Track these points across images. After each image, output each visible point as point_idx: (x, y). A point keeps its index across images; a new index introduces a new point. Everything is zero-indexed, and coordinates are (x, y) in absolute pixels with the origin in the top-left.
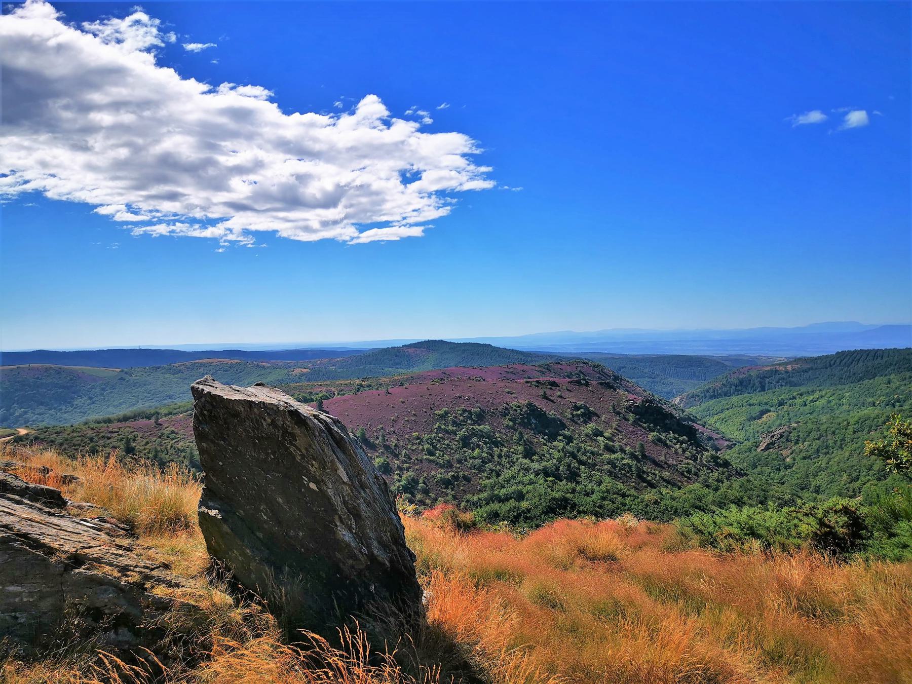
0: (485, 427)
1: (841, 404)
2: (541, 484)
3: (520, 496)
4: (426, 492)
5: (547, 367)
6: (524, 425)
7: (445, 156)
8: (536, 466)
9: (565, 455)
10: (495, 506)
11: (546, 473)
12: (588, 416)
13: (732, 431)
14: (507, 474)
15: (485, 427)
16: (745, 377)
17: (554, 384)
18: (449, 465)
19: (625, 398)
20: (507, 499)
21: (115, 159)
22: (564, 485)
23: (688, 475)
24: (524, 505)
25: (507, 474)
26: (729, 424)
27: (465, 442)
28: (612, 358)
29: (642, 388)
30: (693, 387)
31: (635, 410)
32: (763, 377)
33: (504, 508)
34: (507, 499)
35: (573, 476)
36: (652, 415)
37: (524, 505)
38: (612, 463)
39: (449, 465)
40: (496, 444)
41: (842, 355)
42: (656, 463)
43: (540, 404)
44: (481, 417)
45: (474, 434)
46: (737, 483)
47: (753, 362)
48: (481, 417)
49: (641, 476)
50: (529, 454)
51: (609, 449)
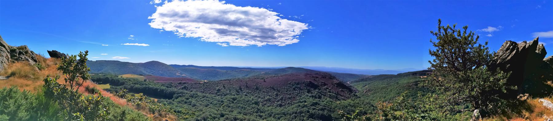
0: (299, 86)
1: (380, 84)
2: (311, 99)
3: (305, 102)
4: (285, 100)
5: (317, 74)
6: (308, 86)
7: (300, 27)
8: (310, 95)
9: (74, 73)
10: (300, 104)
11: (313, 97)
12: (325, 84)
13: (360, 89)
14: (303, 96)
15: (299, 86)
16: (363, 79)
17: (317, 77)
18: (290, 94)
19: (335, 81)
20: (302, 102)
21: (173, 10)
22: (317, 100)
23: (348, 98)
24: (306, 104)
25: (303, 96)
26: (359, 87)
27: (294, 89)
28: (334, 73)
29: (341, 79)
30: (353, 80)
31: (337, 84)
32: (366, 79)
33: (301, 104)
34: (302, 102)
35: (320, 97)
36: (341, 85)
37: (306, 104)
38: (330, 95)
39: (290, 94)
40: (301, 90)
41: (380, 75)
42: (341, 95)
43: (312, 81)
44: (298, 84)
45: (296, 87)
46: (358, 99)
47: (365, 76)
48: (298, 84)
49: (337, 98)
50: (308, 92)
51: (330, 92)
